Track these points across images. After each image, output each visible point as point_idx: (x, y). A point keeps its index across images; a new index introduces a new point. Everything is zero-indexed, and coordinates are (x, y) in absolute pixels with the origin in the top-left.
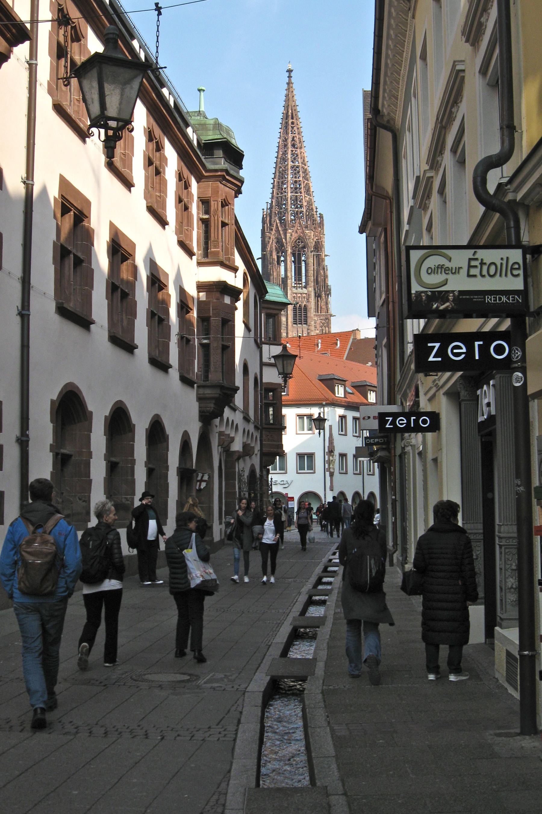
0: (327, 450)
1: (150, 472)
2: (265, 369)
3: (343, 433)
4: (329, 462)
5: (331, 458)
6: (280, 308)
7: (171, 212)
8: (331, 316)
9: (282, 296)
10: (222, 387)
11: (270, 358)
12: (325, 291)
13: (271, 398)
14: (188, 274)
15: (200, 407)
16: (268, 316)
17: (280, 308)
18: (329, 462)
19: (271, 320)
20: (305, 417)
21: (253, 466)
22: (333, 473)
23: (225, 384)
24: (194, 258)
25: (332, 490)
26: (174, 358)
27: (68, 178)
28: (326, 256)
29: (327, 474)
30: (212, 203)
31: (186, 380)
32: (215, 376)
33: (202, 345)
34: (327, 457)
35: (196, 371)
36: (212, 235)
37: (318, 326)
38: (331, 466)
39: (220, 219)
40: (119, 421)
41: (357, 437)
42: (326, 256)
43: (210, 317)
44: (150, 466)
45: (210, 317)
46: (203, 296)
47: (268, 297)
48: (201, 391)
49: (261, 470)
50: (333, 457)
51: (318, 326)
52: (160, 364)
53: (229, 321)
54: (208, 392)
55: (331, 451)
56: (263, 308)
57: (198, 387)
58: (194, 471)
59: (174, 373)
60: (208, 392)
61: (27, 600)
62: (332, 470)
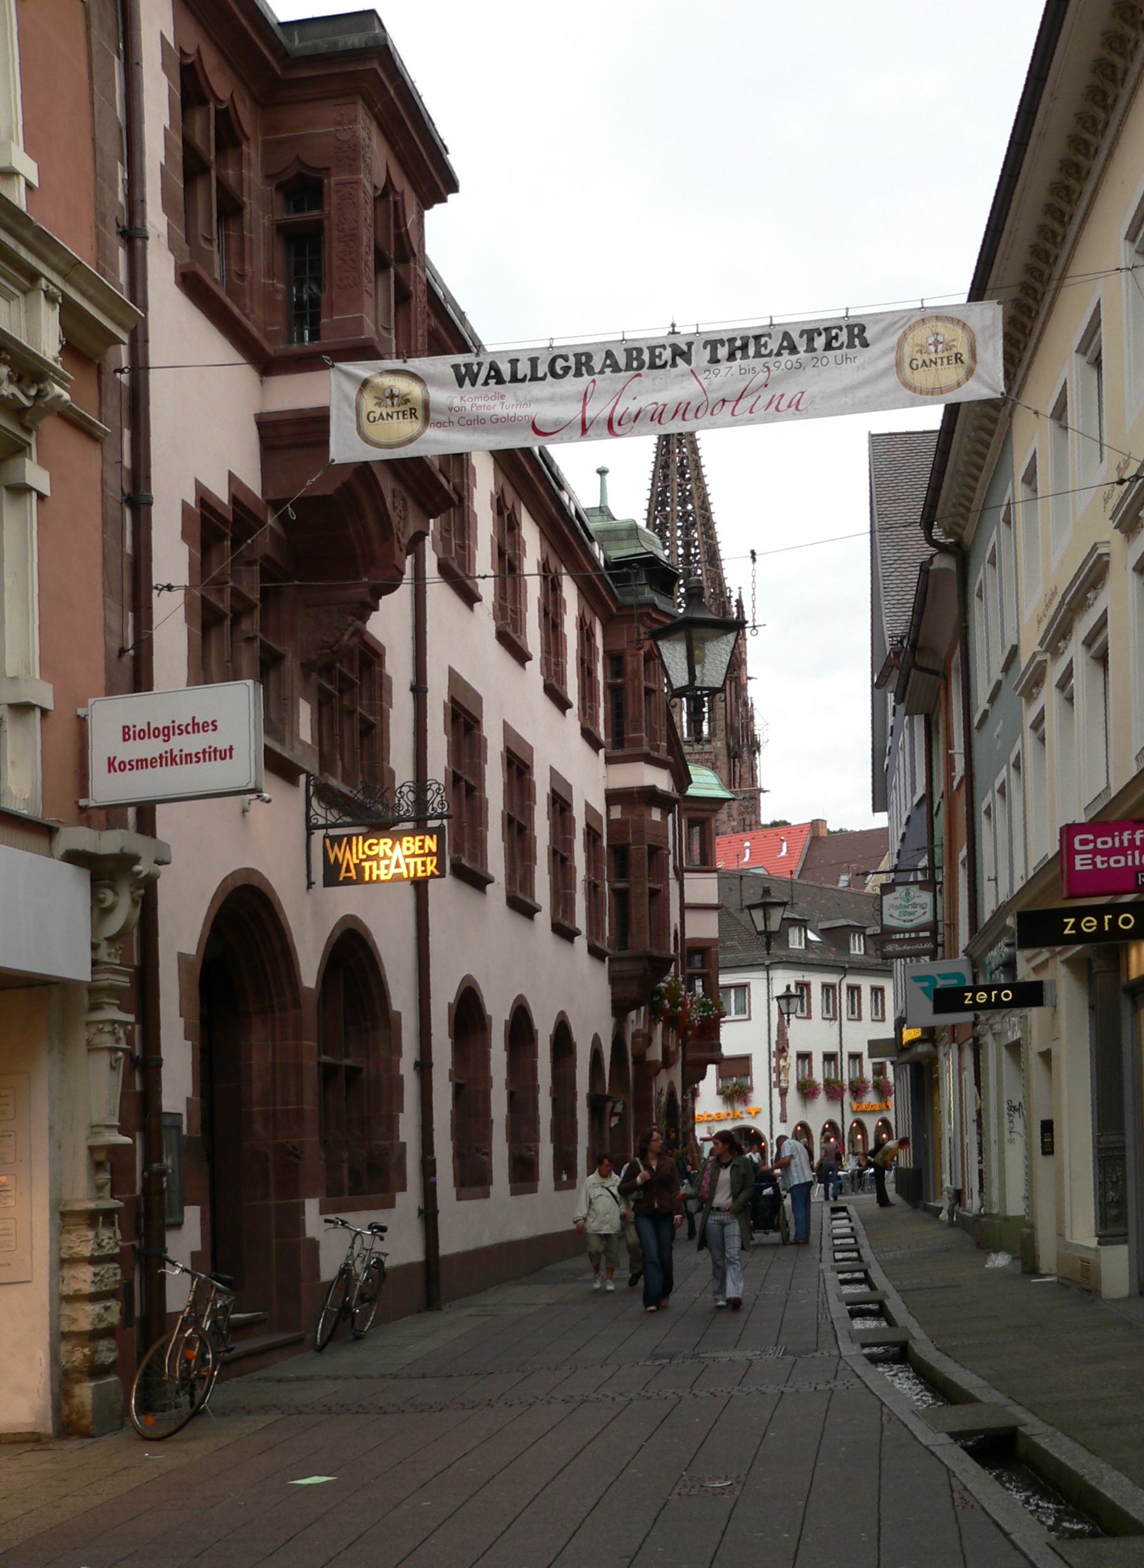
0: (774, 1048)
1: (459, 1092)
2: (688, 916)
3: (805, 1014)
4: (778, 1070)
5: (782, 1063)
6: (714, 807)
7: (572, 691)
8: (761, 790)
9: (717, 787)
10: (651, 959)
11: (742, 910)
12: (748, 745)
13: (699, 965)
14: (590, 779)
15: (613, 994)
16: (692, 823)
17: (714, 807)
18: (778, 1070)
19: (697, 829)
20: (733, 991)
21: (671, 1085)
22: (786, 1089)
23: (656, 953)
24: (602, 752)
25: (785, 1121)
26: (580, 920)
27: (466, 676)
28: (750, 678)
29: (776, 1091)
30: (629, 659)
31: (595, 952)
32: (641, 941)
33: (615, 892)
34: (774, 1060)
35: (607, 934)
36: (630, 711)
37: (735, 815)
38: (782, 1077)
39: (644, 684)
40: (521, 1021)
41: (831, 1020)
42: (750, 678)
43: (629, 844)
44: (459, 1081)
45: (629, 844)
46: (617, 813)
47: (691, 791)
48: (616, 967)
49: (684, 1092)
50: (785, 1059)
51: (735, 815)
52: (564, 932)
53: (661, 848)
54: (627, 967)
55: (782, 1050)
56: (686, 809)
57: (610, 960)
58: (608, 1098)
59: (581, 942)
60: (627, 967)
61: (603, 1273)
62: (783, 1084)
